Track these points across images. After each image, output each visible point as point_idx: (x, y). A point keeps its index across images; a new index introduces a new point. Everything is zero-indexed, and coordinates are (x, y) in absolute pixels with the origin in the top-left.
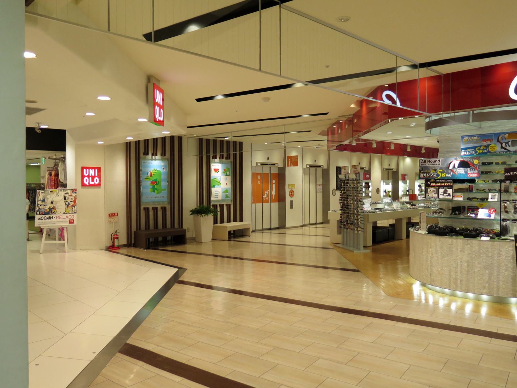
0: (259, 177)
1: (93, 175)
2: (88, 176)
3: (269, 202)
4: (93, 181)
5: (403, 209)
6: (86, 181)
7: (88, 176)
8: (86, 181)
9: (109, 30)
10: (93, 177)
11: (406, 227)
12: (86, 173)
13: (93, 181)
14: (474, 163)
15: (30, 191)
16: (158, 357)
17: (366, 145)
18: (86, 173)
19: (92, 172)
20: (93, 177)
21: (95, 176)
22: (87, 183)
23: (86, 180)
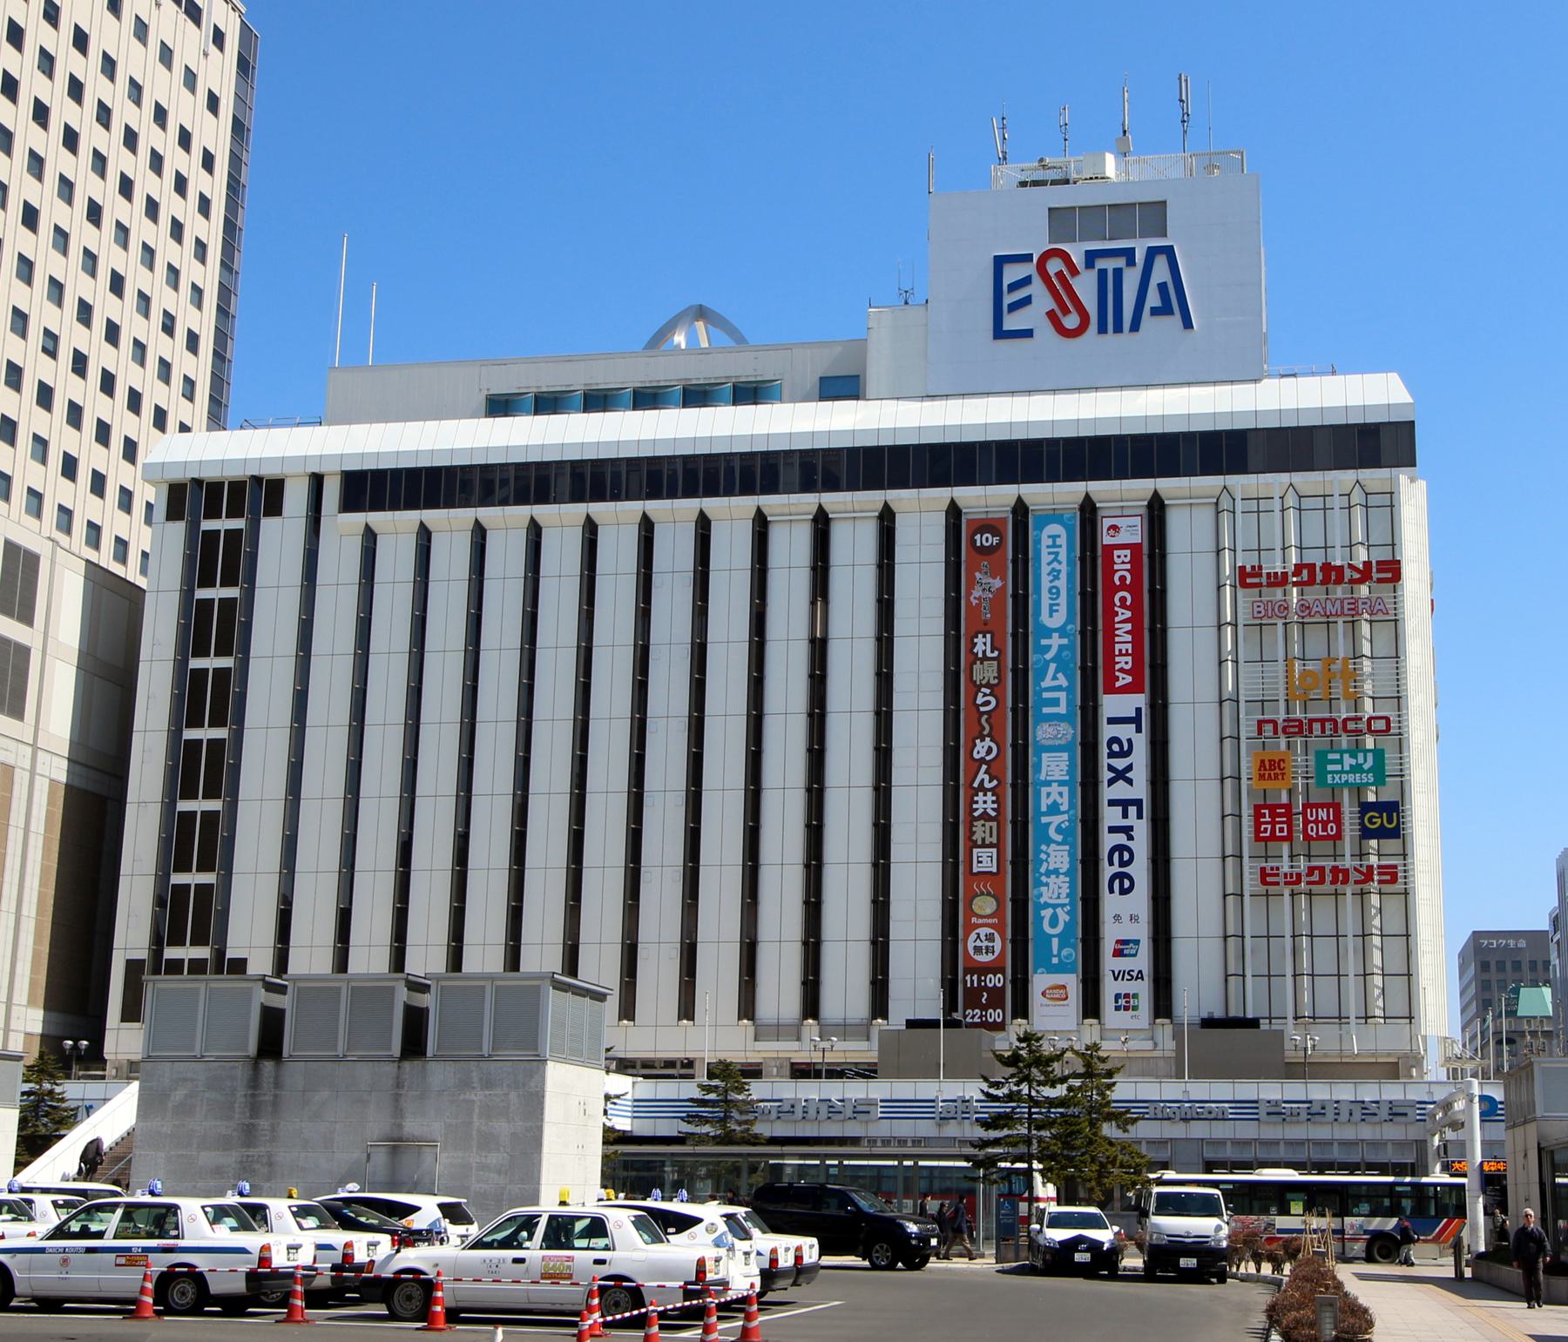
0: (1055, 960)
1: (1325, 819)
2: (1316, 822)
3: (251, 988)
4: (1325, 829)
5: (1014, 1145)
6: (1312, 831)
7: (1316, 822)
8: (1312, 831)
9: (1333, 789)
10: (1325, 824)
11: (605, 1157)
12: (1312, 816)
13: (1325, 829)
14: (810, 1021)
15: (1305, 572)
16: (295, 1209)
17: (626, 1067)
18: (1312, 816)
19: (1322, 814)
20: (1325, 824)
21: (1329, 821)
22: (1314, 834)
23: (1312, 828)
